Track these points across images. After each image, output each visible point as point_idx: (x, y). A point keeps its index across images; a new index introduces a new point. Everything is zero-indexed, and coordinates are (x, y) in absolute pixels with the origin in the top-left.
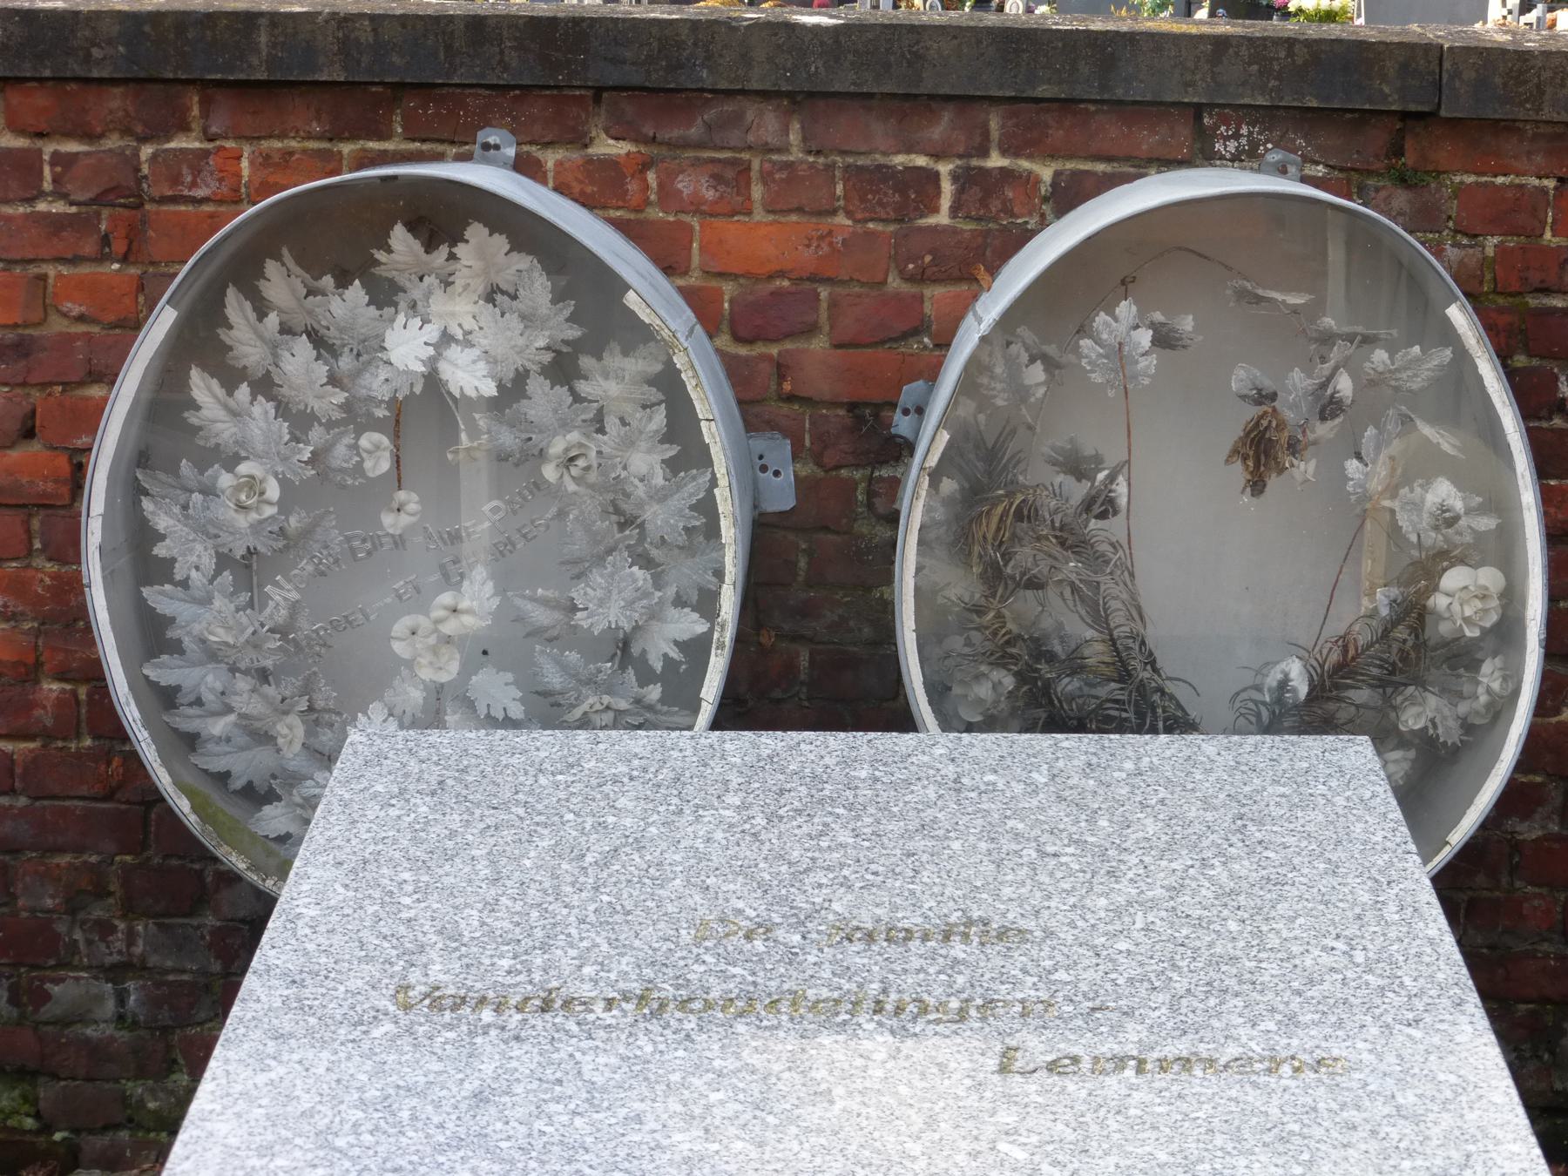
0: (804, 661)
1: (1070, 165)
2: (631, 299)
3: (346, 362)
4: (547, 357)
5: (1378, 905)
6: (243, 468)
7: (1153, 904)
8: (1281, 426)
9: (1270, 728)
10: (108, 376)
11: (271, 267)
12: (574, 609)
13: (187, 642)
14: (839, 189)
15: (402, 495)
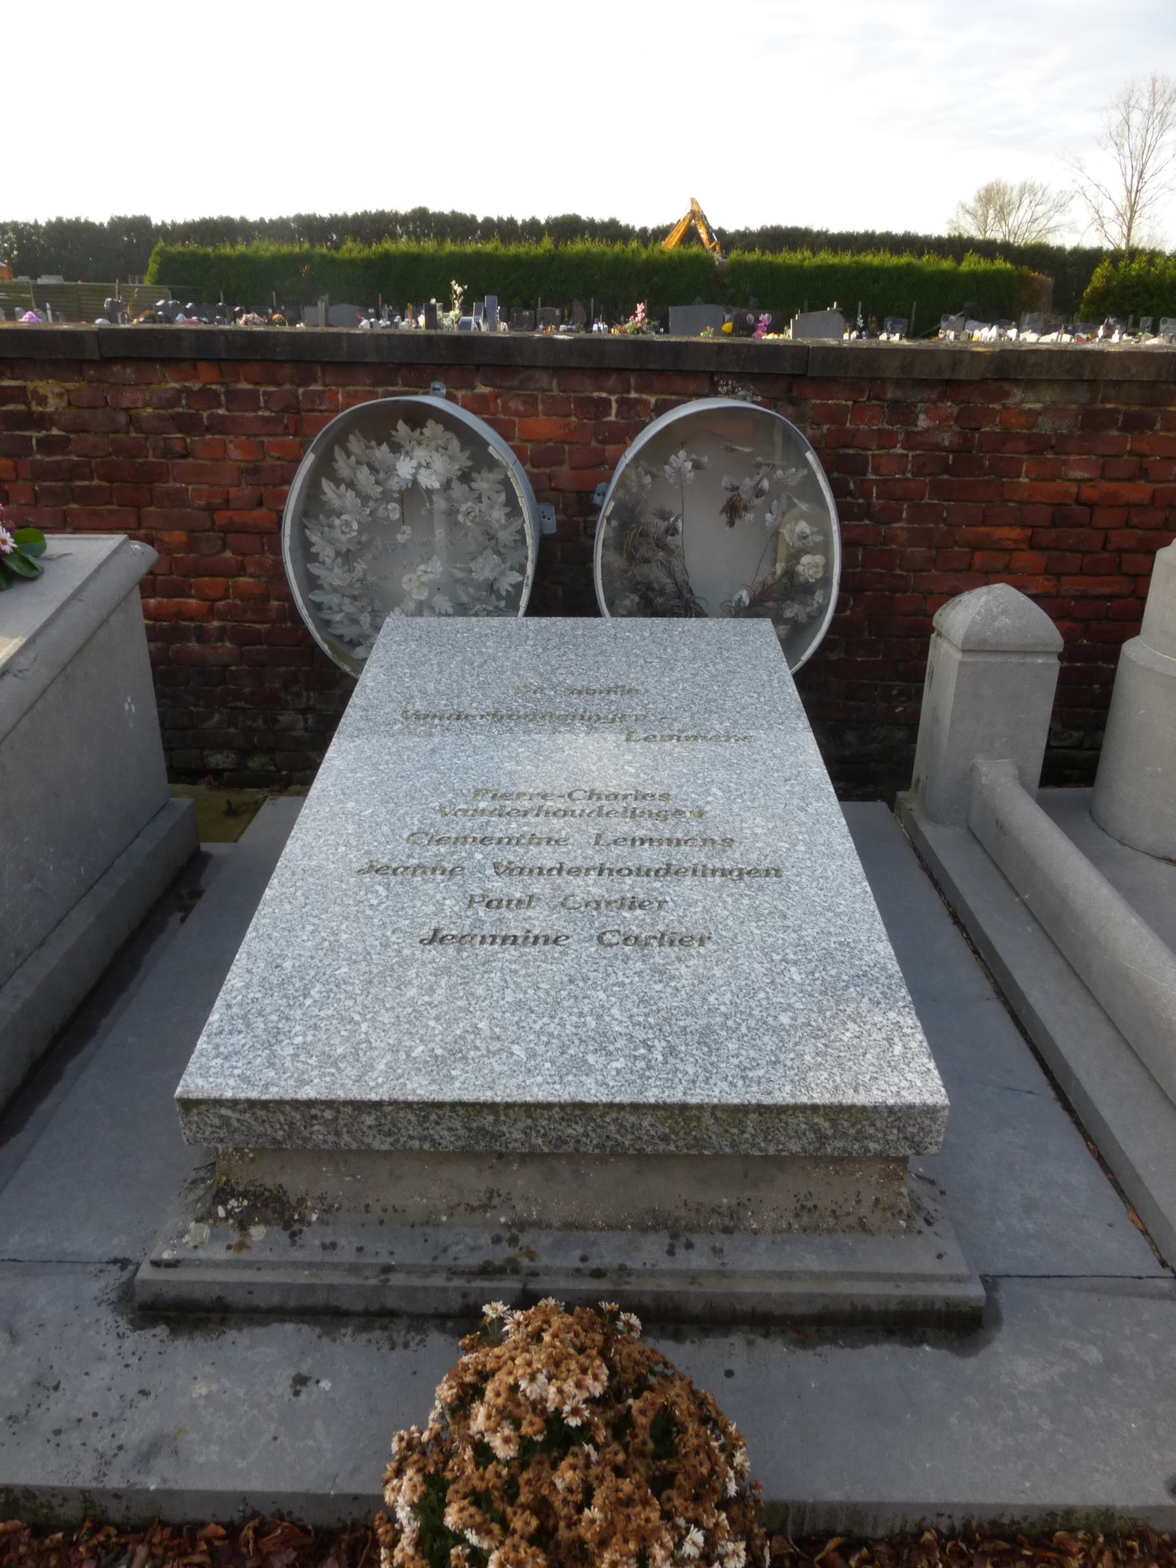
0: (560, 591)
1: (662, 397)
2: (491, 450)
3: (382, 476)
4: (459, 473)
5: (770, 681)
6: (344, 517)
7: (686, 680)
8: (741, 500)
9: (736, 616)
10: (289, 481)
11: (351, 437)
12: (471, 571)
13: (326, 586)
14: (572, 406)
15: (404, 527)
